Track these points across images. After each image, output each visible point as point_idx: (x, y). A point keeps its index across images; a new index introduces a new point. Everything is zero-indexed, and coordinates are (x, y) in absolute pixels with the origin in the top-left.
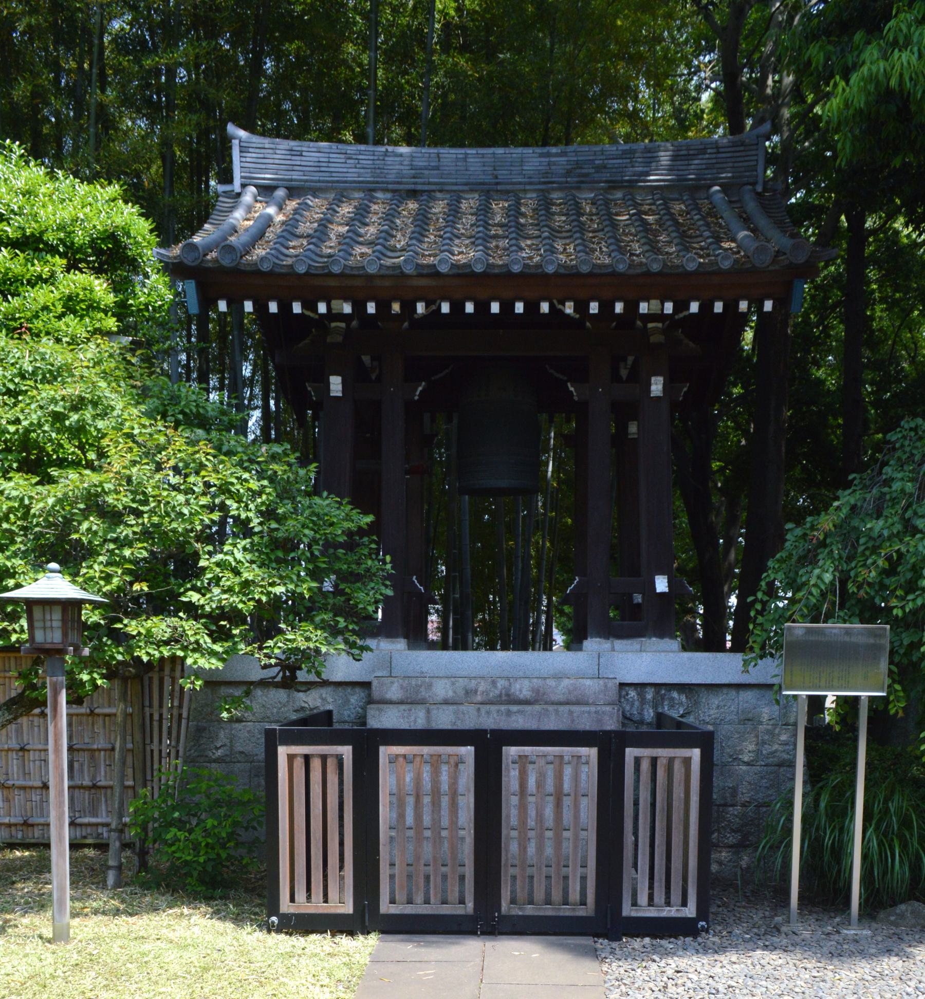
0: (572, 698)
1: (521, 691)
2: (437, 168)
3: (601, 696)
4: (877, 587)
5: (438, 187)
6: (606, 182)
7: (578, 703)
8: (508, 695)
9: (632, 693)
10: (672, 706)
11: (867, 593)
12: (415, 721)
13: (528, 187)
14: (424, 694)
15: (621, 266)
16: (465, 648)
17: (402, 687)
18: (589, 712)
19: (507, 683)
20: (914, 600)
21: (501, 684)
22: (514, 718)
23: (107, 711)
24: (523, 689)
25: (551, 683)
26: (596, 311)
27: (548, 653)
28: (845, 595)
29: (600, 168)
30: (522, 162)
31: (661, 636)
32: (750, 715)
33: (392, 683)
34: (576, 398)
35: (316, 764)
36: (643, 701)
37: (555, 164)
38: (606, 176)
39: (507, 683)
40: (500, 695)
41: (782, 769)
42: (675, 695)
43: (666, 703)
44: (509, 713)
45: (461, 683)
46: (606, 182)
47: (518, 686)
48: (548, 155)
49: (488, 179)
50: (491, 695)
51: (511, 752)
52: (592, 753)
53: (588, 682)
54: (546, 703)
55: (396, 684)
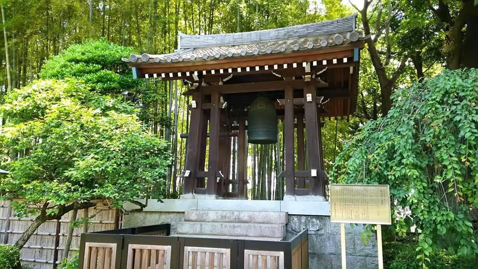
0: (265, 221)
1: (244, 217)
2: (241, 38)
3: (278, 220)
4: (384, 166)
7: (268, 223)
8: (238, 219)
9: (296, 219)
10: (313, 226)
11: (380, 169)
12: (196, 230)
14: (205, 217)
15: (282, 50)
17: (196, 214)
18: (269, 227)
19: (238, 214)
20: (400, 171)
21: (236, 213)
22: (236, 229)
23: (106, 222)
24: (245, 216)
25: (257, 213)
26: (296, 67)
27: (246, 200)
28: (369, 172)
29: (295, 33)
30: (269, 33)
31: (316, 195)
32: (350, 231)
33: (193, 212)
35: (101, 252)
36: (300, 222)
39: (238, 214)
40: (236, 219)
41: (367, 258)
42: (314, 220)
43: (310, 224)
44: (234, 227)
45: (220, 213)
47: (243, 215)
48: (278, 30)
49: (258, 39)
50: (232, 218)
51: (188, 249)
52: (227, 252)
53: (272, 213)
54: (254, 223)
55: (194, 213)
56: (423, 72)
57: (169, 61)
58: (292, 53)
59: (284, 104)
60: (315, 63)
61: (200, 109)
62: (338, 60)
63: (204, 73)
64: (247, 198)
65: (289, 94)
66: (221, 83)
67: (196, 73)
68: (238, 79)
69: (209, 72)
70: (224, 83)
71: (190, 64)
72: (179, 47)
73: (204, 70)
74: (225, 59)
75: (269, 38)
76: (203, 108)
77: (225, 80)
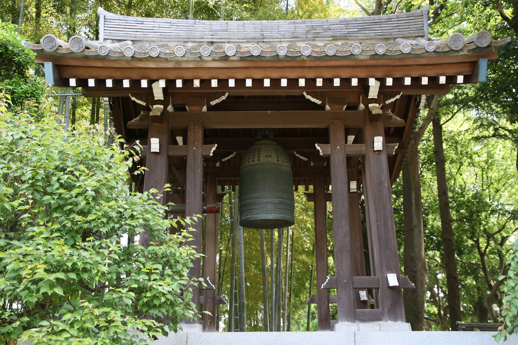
5: (227, 40)
6: (331, 37)
13: (282, 40)
16: (242, 330)
26: (339, 85)
29: (325, 30)
34: (321, 154)
37: (299, 27)
38: (330, 33)
46: (331, 37)
48: (295, 23)
56: (442, 123)
57: (129, 54)
58: (370, 59)
59: (329, 153)
60: (389, 82)
61: (166, 156)
62: (395, 80)
63: (179, 84)
64: (217, 329)
65: (336, 134)
66: (205, 109)
67: (162, 83)
68: (238, 101)
69: (187, 82)
70: (210, 108)
71: (170, 65)
72: (101, 36)
73: (197, 78)
74: (242, 59)
75: (278, 35)
76: (171, 154)
77: (213, 103)
